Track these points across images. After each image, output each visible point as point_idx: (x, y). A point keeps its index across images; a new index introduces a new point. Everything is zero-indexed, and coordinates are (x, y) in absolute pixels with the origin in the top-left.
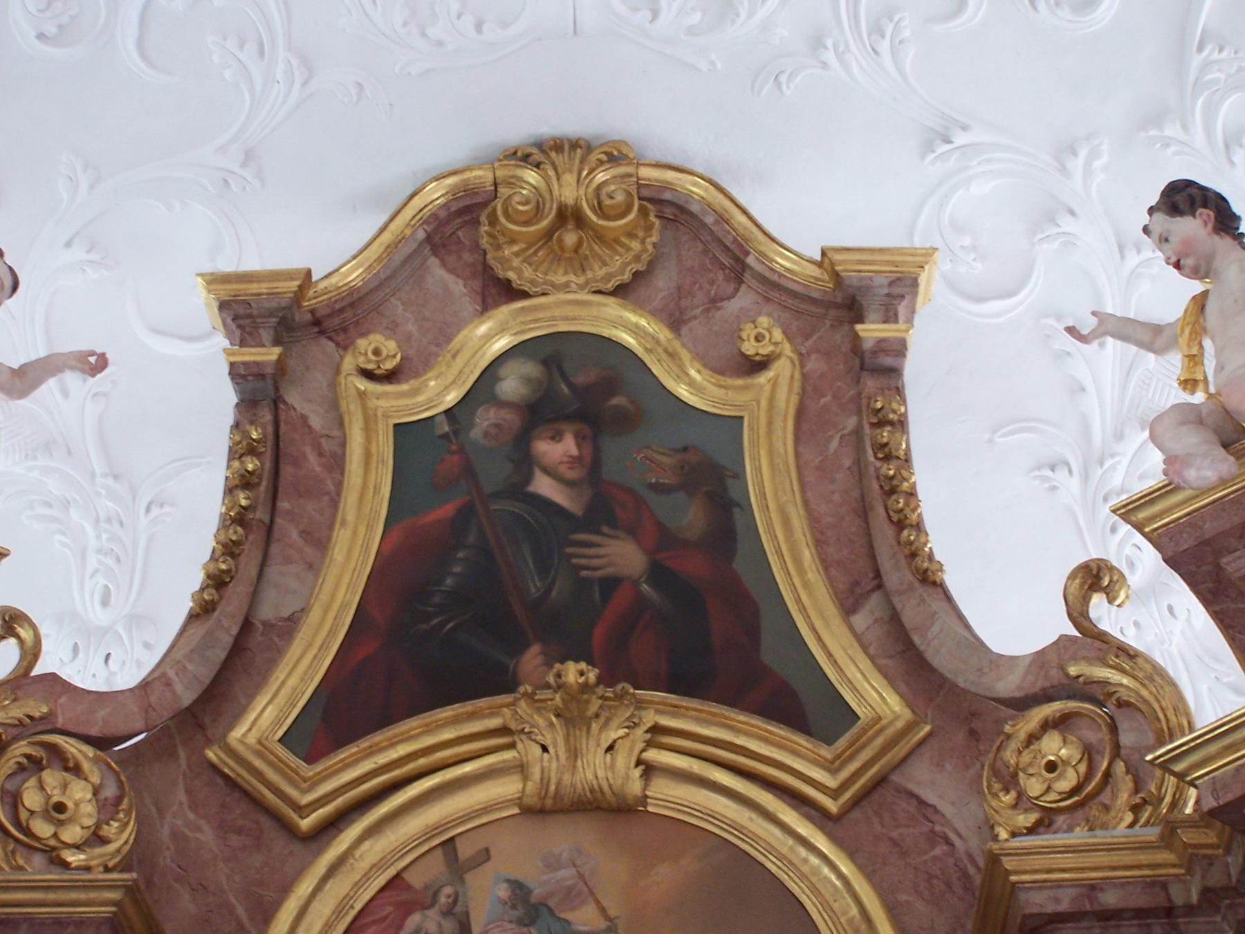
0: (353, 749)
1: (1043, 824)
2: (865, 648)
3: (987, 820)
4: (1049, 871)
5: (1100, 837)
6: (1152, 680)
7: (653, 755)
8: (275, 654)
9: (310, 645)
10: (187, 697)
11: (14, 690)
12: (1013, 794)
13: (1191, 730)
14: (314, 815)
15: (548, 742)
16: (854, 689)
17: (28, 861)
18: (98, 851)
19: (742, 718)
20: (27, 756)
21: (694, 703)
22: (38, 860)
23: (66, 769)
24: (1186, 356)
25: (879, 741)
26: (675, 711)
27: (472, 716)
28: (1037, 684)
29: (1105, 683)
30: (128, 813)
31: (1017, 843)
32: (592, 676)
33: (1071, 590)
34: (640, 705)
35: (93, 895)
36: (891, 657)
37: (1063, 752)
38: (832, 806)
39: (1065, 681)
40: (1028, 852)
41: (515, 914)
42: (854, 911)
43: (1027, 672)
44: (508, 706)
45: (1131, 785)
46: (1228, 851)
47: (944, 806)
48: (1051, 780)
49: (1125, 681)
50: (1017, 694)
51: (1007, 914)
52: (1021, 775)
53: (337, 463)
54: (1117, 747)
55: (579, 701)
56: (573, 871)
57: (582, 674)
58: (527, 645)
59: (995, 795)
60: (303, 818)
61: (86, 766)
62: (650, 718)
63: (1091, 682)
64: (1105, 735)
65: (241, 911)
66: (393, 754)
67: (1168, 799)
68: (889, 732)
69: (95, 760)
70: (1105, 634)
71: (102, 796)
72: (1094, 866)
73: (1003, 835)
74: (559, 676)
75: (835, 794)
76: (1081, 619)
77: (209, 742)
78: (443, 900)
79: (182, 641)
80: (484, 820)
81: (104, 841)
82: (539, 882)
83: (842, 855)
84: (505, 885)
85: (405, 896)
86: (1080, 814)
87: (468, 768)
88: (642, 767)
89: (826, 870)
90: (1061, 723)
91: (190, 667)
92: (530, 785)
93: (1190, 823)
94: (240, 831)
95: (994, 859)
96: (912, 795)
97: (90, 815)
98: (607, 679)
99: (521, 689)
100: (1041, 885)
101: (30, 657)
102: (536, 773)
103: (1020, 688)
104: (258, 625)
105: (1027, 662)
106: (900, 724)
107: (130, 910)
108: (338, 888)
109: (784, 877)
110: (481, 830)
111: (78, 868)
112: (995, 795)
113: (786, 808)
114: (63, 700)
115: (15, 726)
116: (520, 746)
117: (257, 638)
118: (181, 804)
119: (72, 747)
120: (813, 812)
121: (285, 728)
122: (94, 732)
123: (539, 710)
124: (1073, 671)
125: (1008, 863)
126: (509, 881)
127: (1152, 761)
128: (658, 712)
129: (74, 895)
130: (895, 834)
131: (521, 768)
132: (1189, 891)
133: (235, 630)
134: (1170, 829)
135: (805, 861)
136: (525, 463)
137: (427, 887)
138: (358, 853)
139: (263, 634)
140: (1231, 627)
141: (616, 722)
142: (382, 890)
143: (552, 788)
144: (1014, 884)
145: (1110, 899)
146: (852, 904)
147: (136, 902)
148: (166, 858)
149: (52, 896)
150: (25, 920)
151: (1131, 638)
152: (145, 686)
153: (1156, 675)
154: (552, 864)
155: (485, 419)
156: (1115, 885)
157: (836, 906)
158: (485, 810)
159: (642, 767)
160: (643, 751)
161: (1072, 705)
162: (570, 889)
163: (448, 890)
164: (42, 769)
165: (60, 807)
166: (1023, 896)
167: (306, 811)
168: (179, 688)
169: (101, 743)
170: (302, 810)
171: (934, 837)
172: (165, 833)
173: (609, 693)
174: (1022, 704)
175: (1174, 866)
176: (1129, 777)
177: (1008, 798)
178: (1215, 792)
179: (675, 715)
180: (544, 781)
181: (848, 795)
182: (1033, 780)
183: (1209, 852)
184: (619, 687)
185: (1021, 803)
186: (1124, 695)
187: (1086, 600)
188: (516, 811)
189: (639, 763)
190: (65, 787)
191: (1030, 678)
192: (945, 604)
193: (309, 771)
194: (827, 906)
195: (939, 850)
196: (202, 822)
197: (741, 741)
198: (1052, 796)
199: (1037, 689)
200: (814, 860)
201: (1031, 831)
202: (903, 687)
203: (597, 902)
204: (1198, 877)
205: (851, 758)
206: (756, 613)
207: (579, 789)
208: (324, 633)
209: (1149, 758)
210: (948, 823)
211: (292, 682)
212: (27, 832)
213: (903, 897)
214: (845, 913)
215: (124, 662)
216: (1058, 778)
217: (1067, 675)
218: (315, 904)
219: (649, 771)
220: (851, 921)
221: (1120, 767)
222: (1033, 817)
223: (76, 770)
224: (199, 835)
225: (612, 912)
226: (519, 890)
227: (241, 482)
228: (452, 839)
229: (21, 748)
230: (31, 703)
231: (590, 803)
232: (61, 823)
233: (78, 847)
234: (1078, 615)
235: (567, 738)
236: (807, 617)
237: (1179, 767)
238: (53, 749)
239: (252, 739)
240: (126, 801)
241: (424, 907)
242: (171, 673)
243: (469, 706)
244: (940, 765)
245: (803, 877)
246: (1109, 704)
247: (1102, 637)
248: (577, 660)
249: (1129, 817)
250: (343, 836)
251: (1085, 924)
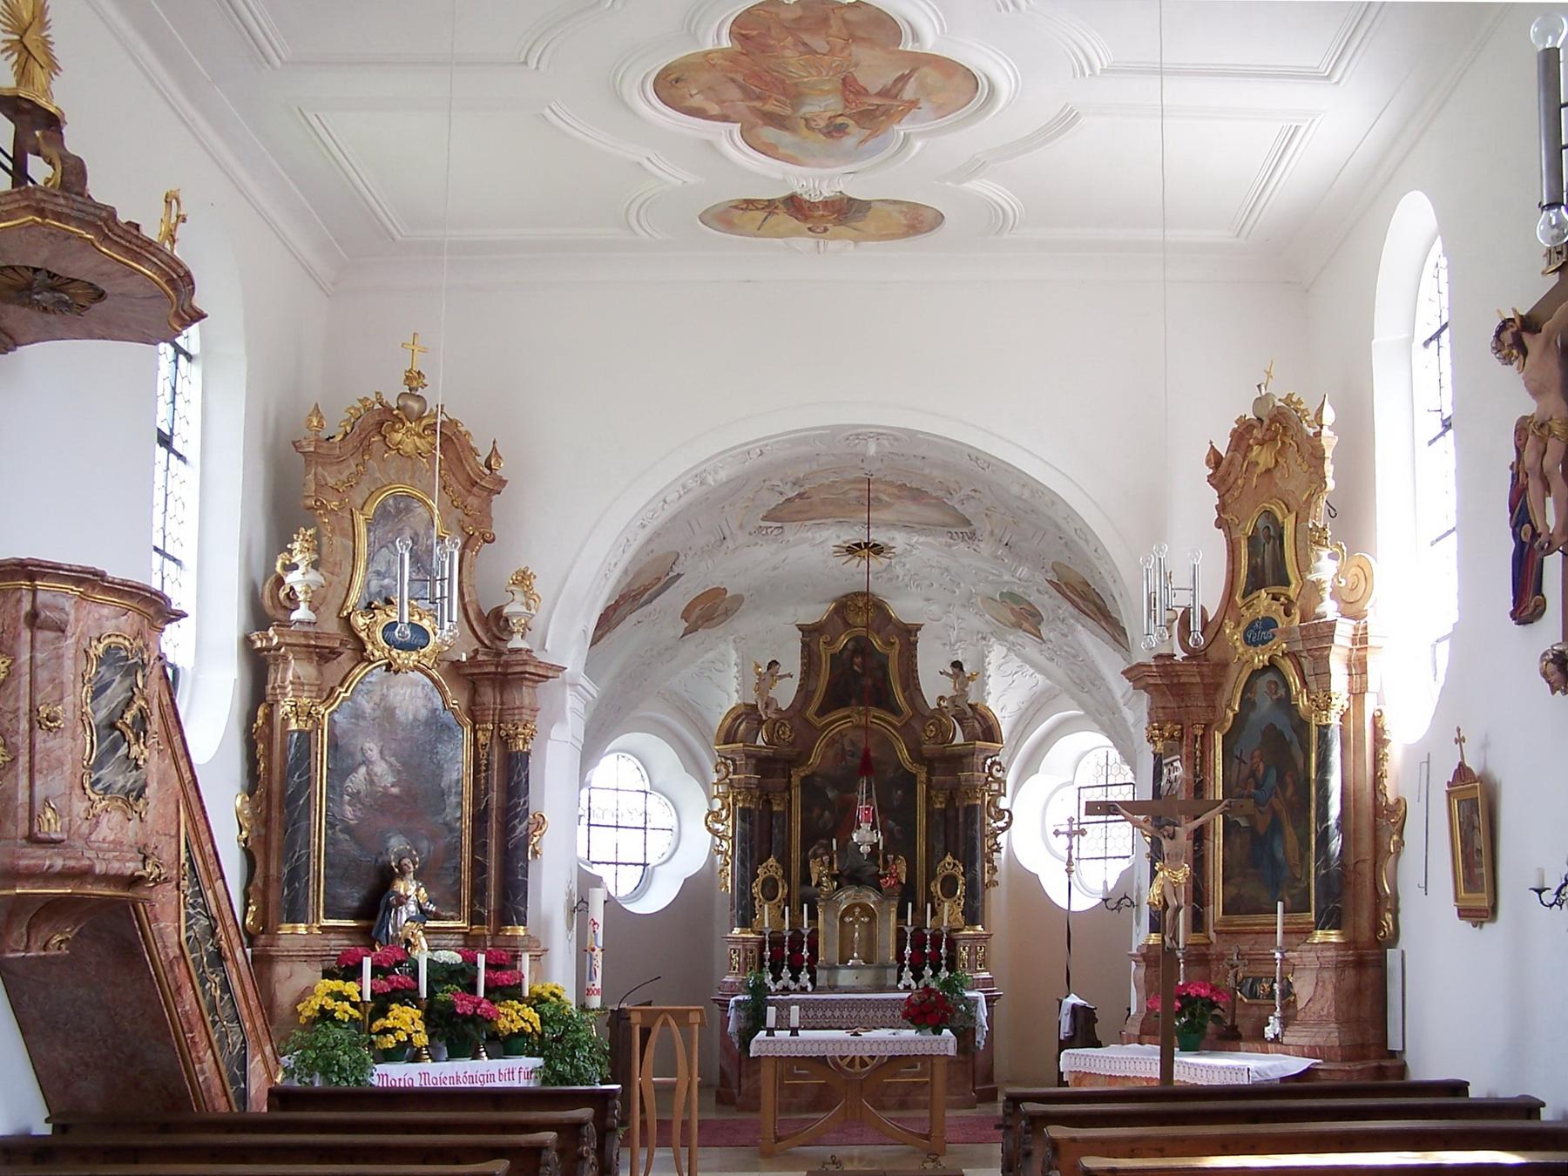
53: (820, 659)
136: (852, 663)
155: (846, 654)
227: (803, 664)
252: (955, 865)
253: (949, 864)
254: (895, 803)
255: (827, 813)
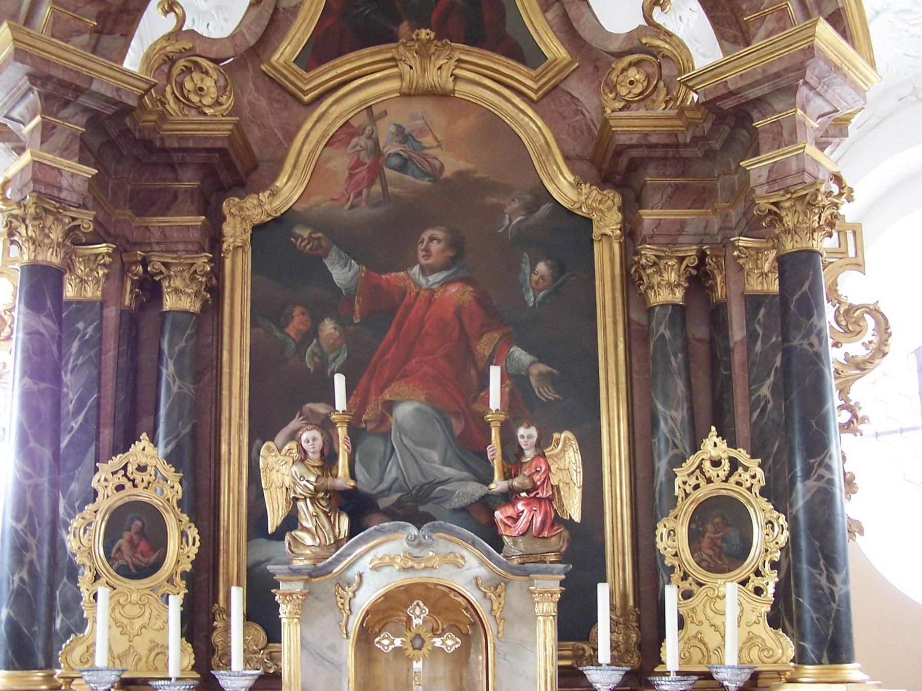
0: (326, 66)
1: (627, 107)
2: (551, 27)
3: (602, 103)
4: (629, 127)
5: (650, 113)
6: (678, 46)
7: (458, 72)
8: (289, 23)
9: (305, 19)
10: (252, 42)
11: (176, 37)
12: (614, 94)
13: (693, 69)
14: (310, 95)
15: (412, 64)
16: (546, 46)
17: (189, 112)
18: (219, 108)
19: (497, 57)
20: (184, 66)
21: (476, 50)
22: (193, 112)
23: (202, 72)
24: (258, 56)
25: (557, 69)
26: (468, 52)
27: (378, 52)
28: (626, 47)
29: (658, 47)
30: (230, 93)
31: (615, 114)
32: (432, 36)
33: (646, 5)
34: (453, 49)
35: (220, 127)
36: (562, 32)
37: (637, 76)
38: (534, 96)
39: (640, 45)
40: (621, 118)
41: (398, 138)
42: (543, 141)
43: (624, 41)
44: (395, 48)
45: (665, 92)
46: (705, 121)
47: (582, 99)
48: (631, 89)
49: (667, 46)
50: (618, 51)
51: (608, 144)
52: (618, 86)
54: (661, 75)
55: (426, 47)
56: (422, 121)
57: (428, 35)
58: (403, 21)
59: (606, 94)
60: (305, 96)
61: (211, 71)
62: (457, 55)
63: (651, 46)
64: (655, 69)
65: (280, 136)
66: (344, 69)
67: (680, 99)
68: (561, 65)
69: (214, 69)
70: (659, 25)
71: (219, 84)
72: (647, 126)
73: (609, 111)
74: (418, 35)
75: (536, 92)
76: (649, 18)
77: (262, 62)
78: (367, 132)
79: (247, 16)
80: (385, 98)
81: (221, 104)
82: (408, 127)
83: (538, 117)
84: (393, 126)
85: (351, 130)
86: (642, 103)
87: (378, 75)
88: (453, 77)
89: (531, 124)
90: (637, 64)
91: (252, 28)
92: (404, 84)
93: (690, 108)
94: (277, 101)
95: (606, 121)
96: (569, 93)
97: (214, 93)
98: (439, 37)
99: (401, 41)
100: (625, 132)
101: (181, 21)
102: (407, 78)
103: (620, 48)
104: (282, 10)
105: (624, 36)
106: (565, 62)
107: (236, 132)
108: (321, 126)
109: (513, 126)
110: (385, 102)
111: (211, 115)
112: (606, 94)
113: (515, 96)
114: (198, 41)
115: (178, 53)
116: (400, 66)
117: (281, 15)
118: (251, 89)
119: (204, 63)
120: (526, 99)
121: (295, 56)
122: (213, 56)
123: (409, 51)
124: (644, 41)
125: (612, 123)
126: (395, 125)
127: (679, 81)
128: (461, 53)
129: (212, 127)
130: (560, 110)
131: (401, 76)
132: (686, 138)
133: (271, 12)
134: (682, 110)
135: (523, 119)
137: (360, 126)
138: (330, 112)
139: (283, 14)
140: (718, 24)
141: (442, 57)
142: (341, 127)
143: (414, 85)
144: (614, 131)
145: (653, 139)
146: (542, 138)
147: (238, 129)
148: (246, 112)
149: (202, 127)
150: (192, 137)
151: (670, 28)
152: (233, 36)
153: (680, 45)
154: (413, 118)
156: (656, 134)
157: (534, 139)
158: (385, 94)
159: (453, 77)
160: (454, 70)
161: (643, 56)
162: (421, 129)
163: (369, 128)
164: (192, 72)
165: (201, 89)
166: (617, 137)
167: (306, 93)
168: (248, 37)
169: (216, 61)
170: (305, 93)
171: (578, 112)
172: (245, 102)
173: (439, 44)
174: (619, 55)
175: (681, 127)
176: (665, 89)
177: (611, 96)
178: (705, 96)
179: (467, 55)
180: (411, 82)
181: (541, 92)
182: (623, 88)
183: (697, 121)
184: (444, 41)
185: (618, 98)
186: (666, 53)
187: (652, 9)
188: (398, 94)
189: (451, 75)
190: (202, 80)
191: (625, 44)
192: (588, 9)
193: (307, 75)
194: (531, 139)
195: (579, 117)
196: (261, 98)
197: (496, 67)
198: (631, 95)
199: (627, 49)
200: (527, 119)
201: (620, 110)
202: (567, 46)
203: (433, 135)
204: (691, 130)
205: (543, 76)
206: (504, 10)
207: (426, 86)
208: (311, 14)
209: (679, 79)
210: (583, 106)
211: (298, 35)
212: (188, 100)
213: (563, 137)
214: (538, 142)
215: (215, 28)
216: (634, 88)
217: (641, 43)
218: (312, 133)
219: (456, 78)
220: (540, 146)
221: (661, 84)
222: (622, 104)
223: (206, 73)
224: (260, 103)
225: (439, 139)
226: (400, 128)
228: (371, 106)
229: (181, 63)
230: (184, 42)
231: (430, 92)
232: (201, 96)
233: (209, 106)
234: (648, 17)
235: (421, 63)
236: (527, 13)
237: (690, 84)
238: (196, 63)
239: (281, 61)
240: (229, 87)
241: (359, 135)
242: (244, 30)
243: (377, 48)
244: (581, 81)
245: (521, 126)
246: (659, 57)
247: (658, 26)
248: (426, 28)
249: (664, 106)
250: (323, 104)
251: (641, 149)
252: (734, 464)
253: (716, 463)
254: (530, 298)
255: (328, 327)
